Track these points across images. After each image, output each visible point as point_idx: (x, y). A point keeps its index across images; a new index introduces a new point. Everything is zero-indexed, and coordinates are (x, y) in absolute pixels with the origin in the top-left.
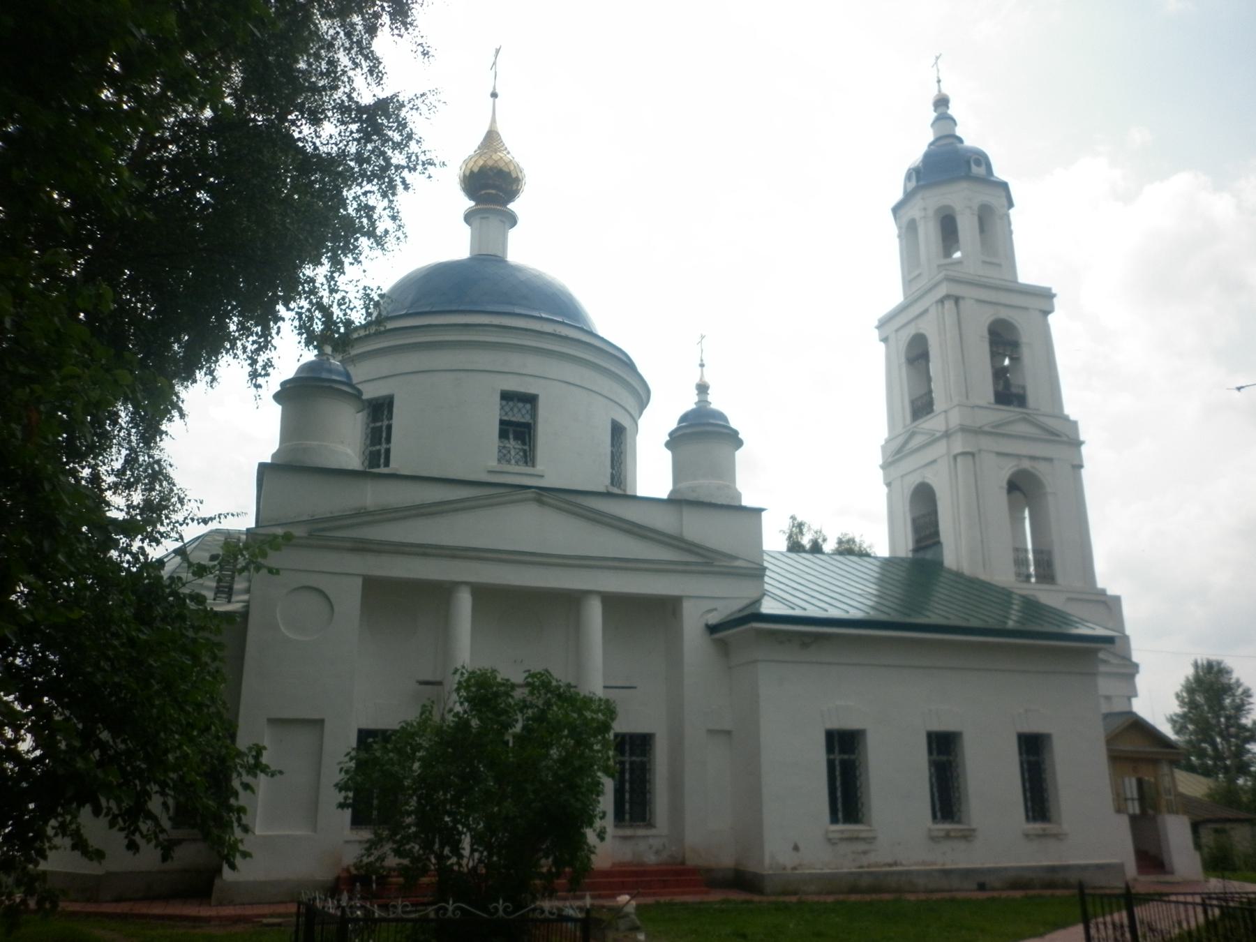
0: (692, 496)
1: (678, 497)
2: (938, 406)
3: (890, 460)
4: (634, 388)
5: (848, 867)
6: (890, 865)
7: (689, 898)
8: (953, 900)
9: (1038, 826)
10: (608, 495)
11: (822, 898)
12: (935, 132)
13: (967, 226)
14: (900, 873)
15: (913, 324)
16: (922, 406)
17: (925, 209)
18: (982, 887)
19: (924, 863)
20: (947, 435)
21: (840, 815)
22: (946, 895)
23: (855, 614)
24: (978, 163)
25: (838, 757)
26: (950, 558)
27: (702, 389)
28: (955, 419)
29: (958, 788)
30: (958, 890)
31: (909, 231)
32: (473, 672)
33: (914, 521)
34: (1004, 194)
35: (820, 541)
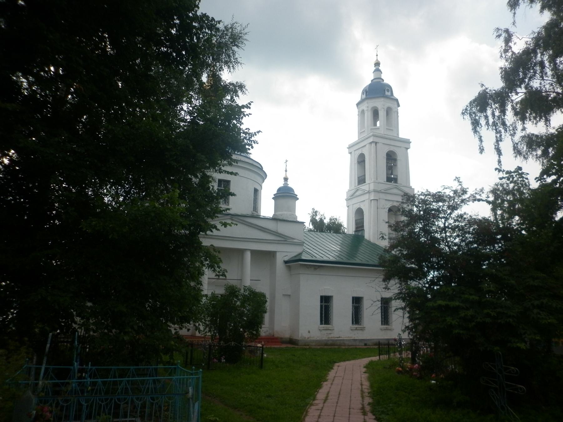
0: (281, 218)
1: (276, 217)
2: (367, 181)
3: (349, 198)
4: (262, 176)
5: (325, 338)
6: (338, 338)
7: (276, 346)
8: (356, 348)
9: (385, 326)
10: (252, 217)
11: (316, 347)
12: (374, 76)
13: (382, 114)
14: (341, 340)
15: (361, 149)
16: (361, 180)
17: (368, 107)
18: (366, 345)
19: (348, 337)
20: (369, 192)
21: (323, 322)
22: (354, 347)
23: (332, 259)
24: (388, 91)
25: (324, 304)
26: (367, 236)
27: (286, 179)
28: (372, 187)
29: (361, 314)
30: (359, 345)
31: (362, 113)
32: (230, 286)
33: (356, 220)
34: (396, 103)
35: (323, 218)
